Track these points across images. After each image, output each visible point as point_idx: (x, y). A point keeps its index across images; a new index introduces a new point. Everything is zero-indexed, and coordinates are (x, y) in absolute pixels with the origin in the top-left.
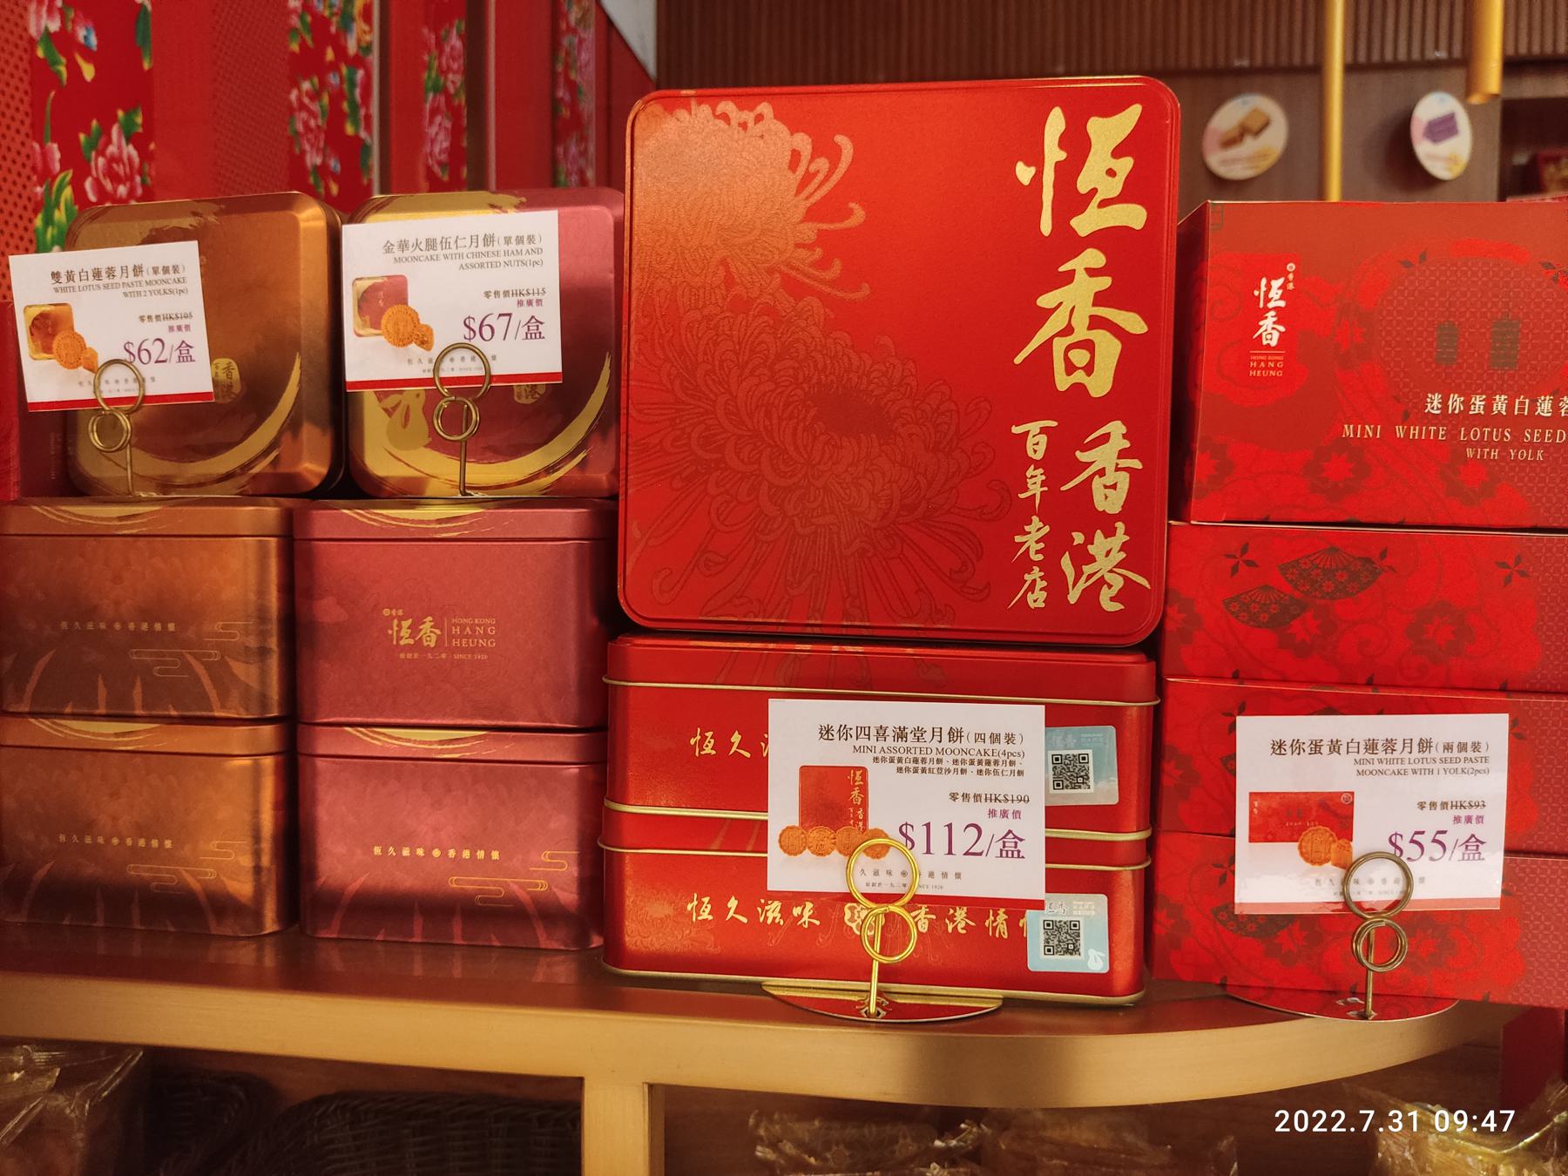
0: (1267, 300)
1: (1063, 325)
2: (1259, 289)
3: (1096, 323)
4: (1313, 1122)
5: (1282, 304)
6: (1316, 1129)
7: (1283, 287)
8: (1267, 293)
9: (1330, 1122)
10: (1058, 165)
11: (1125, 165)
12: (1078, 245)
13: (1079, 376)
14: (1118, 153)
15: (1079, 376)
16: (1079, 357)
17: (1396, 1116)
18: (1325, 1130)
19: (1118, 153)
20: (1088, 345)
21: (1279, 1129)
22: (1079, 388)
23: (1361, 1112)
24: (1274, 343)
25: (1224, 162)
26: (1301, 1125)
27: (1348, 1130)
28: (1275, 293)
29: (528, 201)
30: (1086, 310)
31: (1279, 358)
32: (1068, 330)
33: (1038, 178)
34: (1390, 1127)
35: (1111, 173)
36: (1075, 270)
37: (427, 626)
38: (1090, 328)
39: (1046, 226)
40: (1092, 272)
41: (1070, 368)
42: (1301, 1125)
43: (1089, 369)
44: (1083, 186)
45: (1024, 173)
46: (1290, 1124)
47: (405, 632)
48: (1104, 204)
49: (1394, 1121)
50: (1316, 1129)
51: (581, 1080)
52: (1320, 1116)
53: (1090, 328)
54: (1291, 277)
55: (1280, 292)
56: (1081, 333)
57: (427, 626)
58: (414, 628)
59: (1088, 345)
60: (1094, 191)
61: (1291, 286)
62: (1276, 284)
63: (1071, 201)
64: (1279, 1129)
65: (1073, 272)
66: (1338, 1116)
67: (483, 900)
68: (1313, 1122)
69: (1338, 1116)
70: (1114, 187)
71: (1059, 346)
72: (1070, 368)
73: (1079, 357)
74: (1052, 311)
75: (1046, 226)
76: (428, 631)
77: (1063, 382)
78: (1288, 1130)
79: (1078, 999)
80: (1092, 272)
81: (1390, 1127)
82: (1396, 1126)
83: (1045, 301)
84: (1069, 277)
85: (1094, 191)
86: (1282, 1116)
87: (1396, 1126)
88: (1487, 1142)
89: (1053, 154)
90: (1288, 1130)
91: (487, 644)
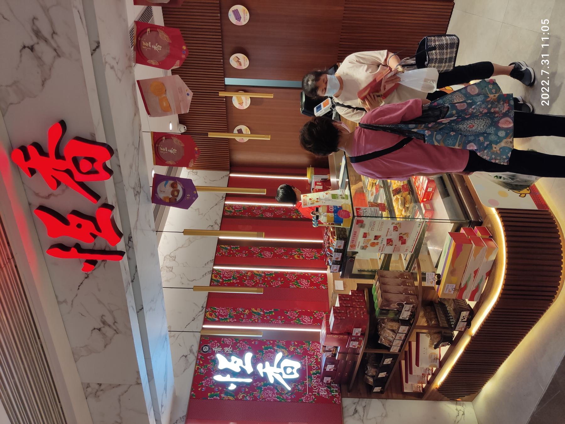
2: (228, 384)
3: (279, 366)
6: (548, 91)
8: (147, 47)
9: (546, 86)
11: (146, 43)
12: (151, 47)
14: (229, 360)
15: (295, 371)
16: (289, 370)
17: (543, 62)
19: (229, 360)
20: (285, 368)
21: (548, 104)
22: (299, 371)
25: (245, 66)
27: (548, 79)
29: (244, 250)
30: (275, 369)
32: (281, 374)
33: (147, 49)
34: (548, 64)
35: (235, 362)
36: (263, 372)
38: (280, 368)
39: (150, 49)
40: (264, 367)
41: (292, 373)
43: (292, 368)
44: (148, 46)
45: (147, 50)
46: (546, 100)
48: (244, 364)
49: (545, 63)
50: (548, 91)
52: (543, 90)
53: (280, 368)
55: (233, 358)
56: (282, 370)
59: (285, 368)
60: (240, 367)
63: (243, 373)
64: (548, 104)
66: (543, 83)
67: (471, 173)
69: (543, 83)
70: (240, 361)
71: (285, 376)
72: (292, 373)
74: (275, 379)
75: (150, 49)
77: (296, 376)
78: (548, 101)
79: (501, 236)
80: (264, 367)
81: (548, 64)
82: (547, 62)
83: (155, 50)
84: (265, 374)
85: (240, 367)
86: (543, 103)
87: (547, 62)
88: (545, 391)
90: (548, 101)
91: (315, 379)
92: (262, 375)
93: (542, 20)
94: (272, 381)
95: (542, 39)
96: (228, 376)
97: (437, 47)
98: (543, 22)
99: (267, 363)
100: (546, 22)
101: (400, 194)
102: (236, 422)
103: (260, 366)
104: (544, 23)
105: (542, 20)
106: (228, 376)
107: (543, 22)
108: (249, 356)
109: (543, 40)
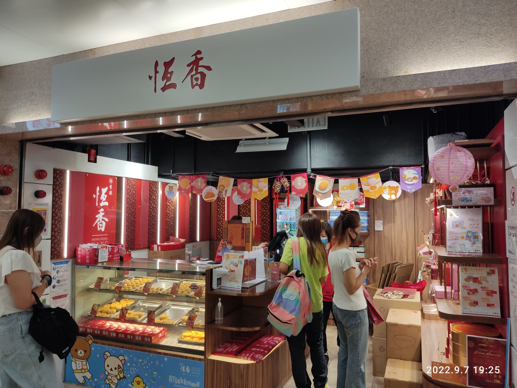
0: (100, 201)
1: (99, 220)
2: (96, 194)
3: (103, 220)
4: (439, 370)
5: (106, 204)
6: (440, 373)
7: (107, 193)
8: (100, 196)
10: (98, 195)
13: (101, 228)
14: (105, 194)
16: (101, 225)
18: (443, 373)
19: (105, 194)
20: (102, 223)
22: (101, 230)
23: (476, 373)
24: (103, 229)
26: (435, 371)
27: (451, 373)
28: (103, 197)
30: (102, 218)
31: (105, 239)
34: (496, 372)
37: (188, 368)
40: (102, 212)
42: (435, 371)
43: (102, 227)
45: (94, 196)
47: (183, 369)
48: (104, 201)
50: (440, 373)
51: (163, 92)
54: (111, 187)
55: (106, 196)
56: (101, 221)
57: (188, 368)
58: (185, 369)
59: (102, 223)
61: (111, 193)
62: (104, 190)
65: (100, 212)
68: (439, 370)
70: (104, 199)
71: (98, 223)
72: (100, 227)
73: (101, 225)
76: (101, 220)
77: (99, 229)
80: (102, 212)
81: (496, 372)
84: (99, 213)
89: (98, 194)
92: (99, 211)
93: (499, 367)
94: (97, 216)
95: (476, 367)
96: (99, 194)
97: (156, 313)
98: (497, 368)
99: (103, 214)
100: (497, 371)
101: (143, 287)
102: (153, 164)
103: (102, 210)
104: (496, 369)
105: (499, 367)
106: (99, 194)
107: (497, 368)
108: (106, 204)
109: (474, 368)
